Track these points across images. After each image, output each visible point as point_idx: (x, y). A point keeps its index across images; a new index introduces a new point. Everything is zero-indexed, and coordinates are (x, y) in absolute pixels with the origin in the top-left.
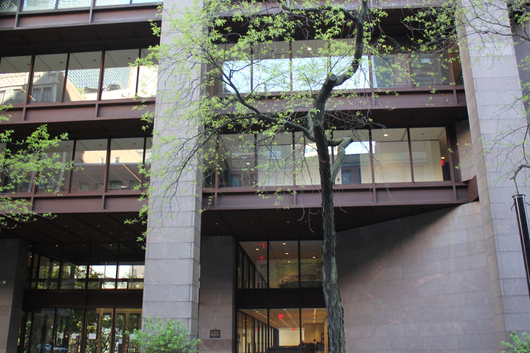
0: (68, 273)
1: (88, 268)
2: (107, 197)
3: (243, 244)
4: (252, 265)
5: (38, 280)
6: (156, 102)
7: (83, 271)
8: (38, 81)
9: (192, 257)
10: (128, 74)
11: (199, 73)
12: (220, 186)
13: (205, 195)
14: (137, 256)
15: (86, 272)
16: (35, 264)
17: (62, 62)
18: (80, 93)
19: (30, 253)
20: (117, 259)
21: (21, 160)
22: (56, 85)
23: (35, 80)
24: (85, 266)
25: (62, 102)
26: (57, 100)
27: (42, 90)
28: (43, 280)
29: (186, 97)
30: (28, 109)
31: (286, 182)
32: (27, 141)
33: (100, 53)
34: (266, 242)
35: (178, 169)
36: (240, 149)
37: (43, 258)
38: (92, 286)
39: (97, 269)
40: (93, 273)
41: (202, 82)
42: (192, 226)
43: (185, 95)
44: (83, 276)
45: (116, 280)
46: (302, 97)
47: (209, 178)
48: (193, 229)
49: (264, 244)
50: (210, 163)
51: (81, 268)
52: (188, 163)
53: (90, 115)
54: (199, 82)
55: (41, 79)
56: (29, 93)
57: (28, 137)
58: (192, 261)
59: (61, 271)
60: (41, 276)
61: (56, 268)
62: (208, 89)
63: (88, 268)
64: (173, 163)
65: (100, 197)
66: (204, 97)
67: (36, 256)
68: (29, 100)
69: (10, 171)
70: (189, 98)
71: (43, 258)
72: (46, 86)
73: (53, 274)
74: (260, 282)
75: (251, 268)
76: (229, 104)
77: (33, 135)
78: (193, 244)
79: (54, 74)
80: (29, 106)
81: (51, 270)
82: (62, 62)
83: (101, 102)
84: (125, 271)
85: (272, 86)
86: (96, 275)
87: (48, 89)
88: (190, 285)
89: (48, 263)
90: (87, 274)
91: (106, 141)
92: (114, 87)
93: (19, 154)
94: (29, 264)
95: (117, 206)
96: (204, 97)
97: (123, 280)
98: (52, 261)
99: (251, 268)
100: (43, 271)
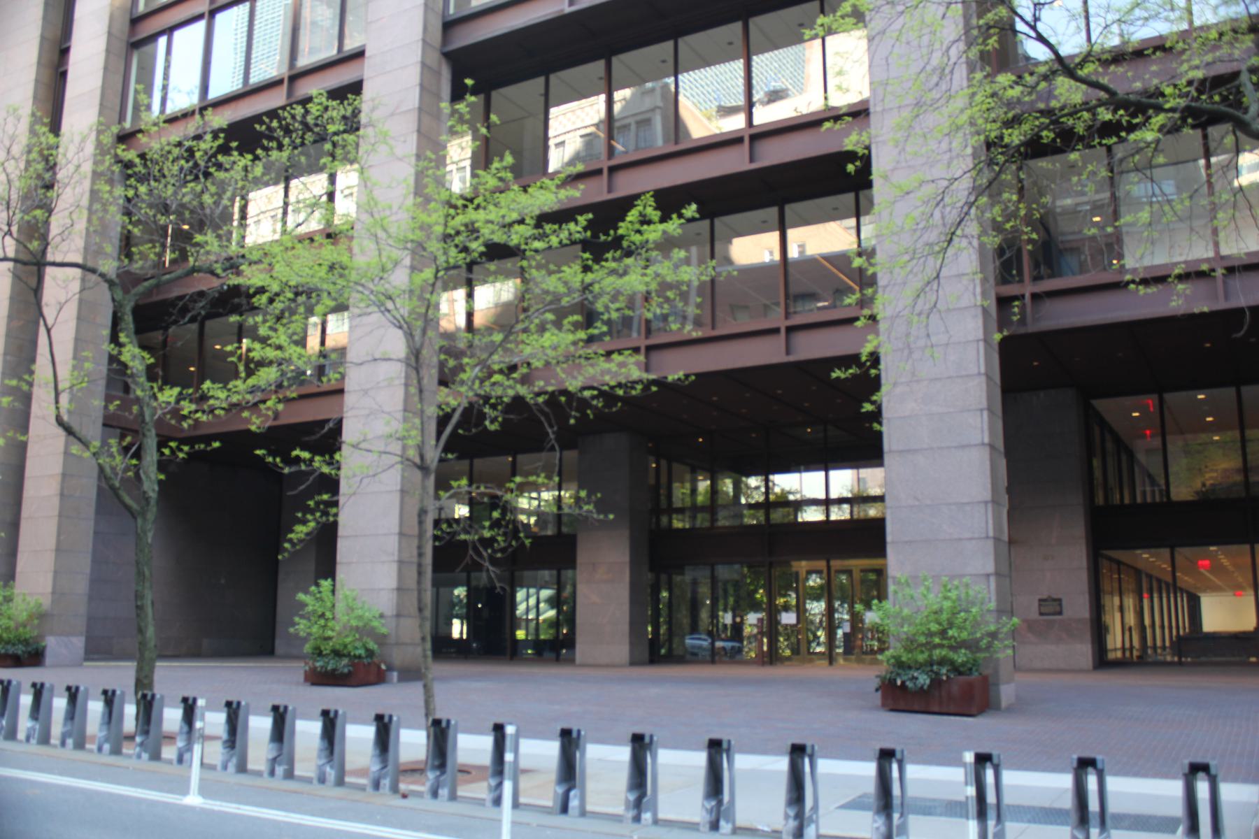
0: (727, 493)
1: (767, 481)
2: (790, 330)
3: (1101, 405)
4: (1124, 450)
5: (672, 510)
6: (872, 110)
7: (757, 488)
8: (624, 109)
9: (986, 440)
10: (801, 63)
11: (961, 26)
12: (1036, 278)
13: (1003, 303)
14: (863, 446)
15: (763, 489)
16: (664, 480)
17: (664, 61)
18: (709, 119)
19: (651, 458)
20: (825, 459)
21: (613, 272)
22: (658, 111)
23: (617, 108)
24: (760, 478)
25: (647, 337)
26: (666, 141)
27: (633, 127)
28: (681, 511)
29: (937, 85)
30: (613, 170)
31: (1198, 251)
32: (620, 232)
33: (737, 27)
34: (1155, 397)
35: (937, 248)
36: (1075, 187)
37: (676, 467)
38: (777, 516)
39: (785, 482)
40: (777, 490)
41: (969, 45)
42: (979, 374)
43: (935, 79)
44: (758, 497)
45: (827, 503)
46: (1221, 35)
47: (1006, 262)
48: (983, 379)
49: (1151, 401)
50: (1008, 226)
51: (753, 481)
52: (959, 232)
53: (734, 162)
54: (962, 46)
55: (627, 103)
56: (610, 136)
57: (621, 224)
58: (987, 449)
59: (714, 491)
60: (677, 503)
61: (704, 485)
62: (984, 56)
63: (767, 481)
64: (925, 238)
65: (776, 331)
66: (979, 75)
67: (663, 463)
68: (611, 151)
69: (596, 297)
70: (944, 87)
71: (676, 466)
72: (639, 118)
73: (700, 499)
74: (1148, 489)
75: (1124, 458)
76: (1038, 84)
77: (628, 219)
78: (985, 414)
79: (653, 90)
80: (615, 162)
81: (694, 491)
82: (664, 61)
83: (753, 131)
84: (843, 481)
85: (1140, 23)
86: (784, 493)
87: (644, 123)
88: (986, 503)
89: (688, 476)
90: (767, 493)
91: (773, 212)
92: (775, 96)
93: (606, 260)
94: (652, 481)
95: (812, 347)
96: (979, 75)
97: (841, 501)
98: (694, 470)
99: (1124, 458)
100: (680, 492)
